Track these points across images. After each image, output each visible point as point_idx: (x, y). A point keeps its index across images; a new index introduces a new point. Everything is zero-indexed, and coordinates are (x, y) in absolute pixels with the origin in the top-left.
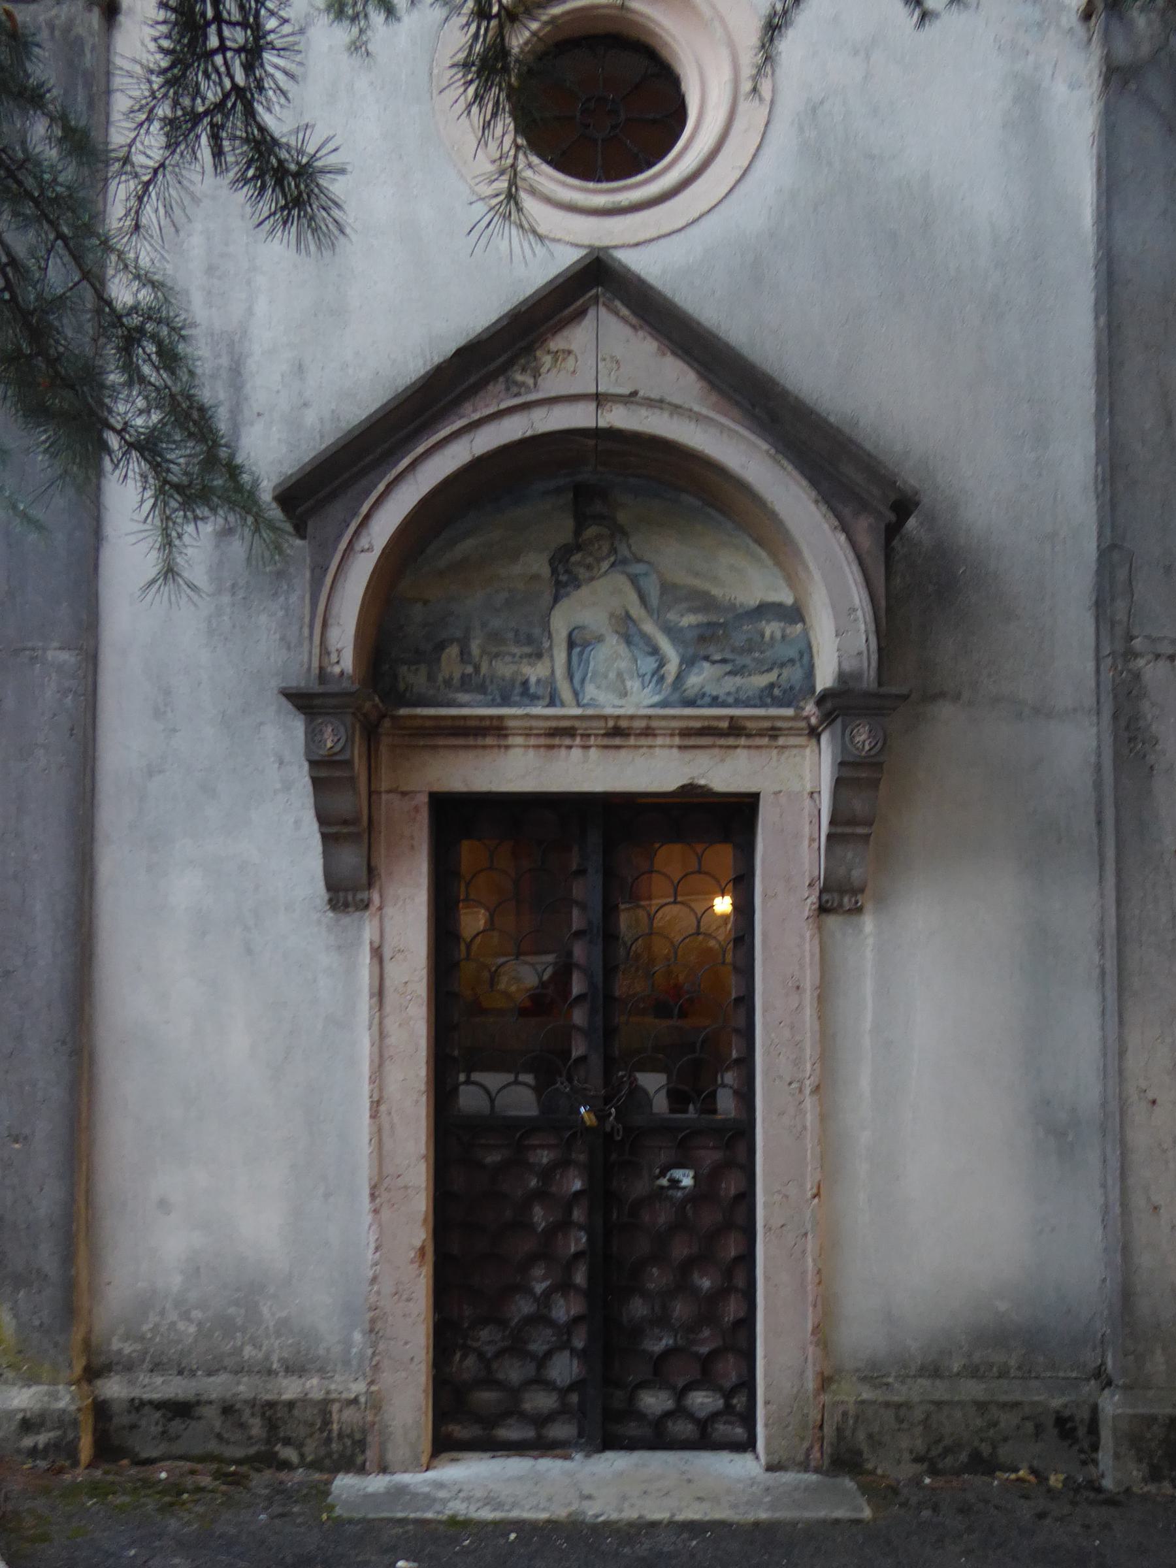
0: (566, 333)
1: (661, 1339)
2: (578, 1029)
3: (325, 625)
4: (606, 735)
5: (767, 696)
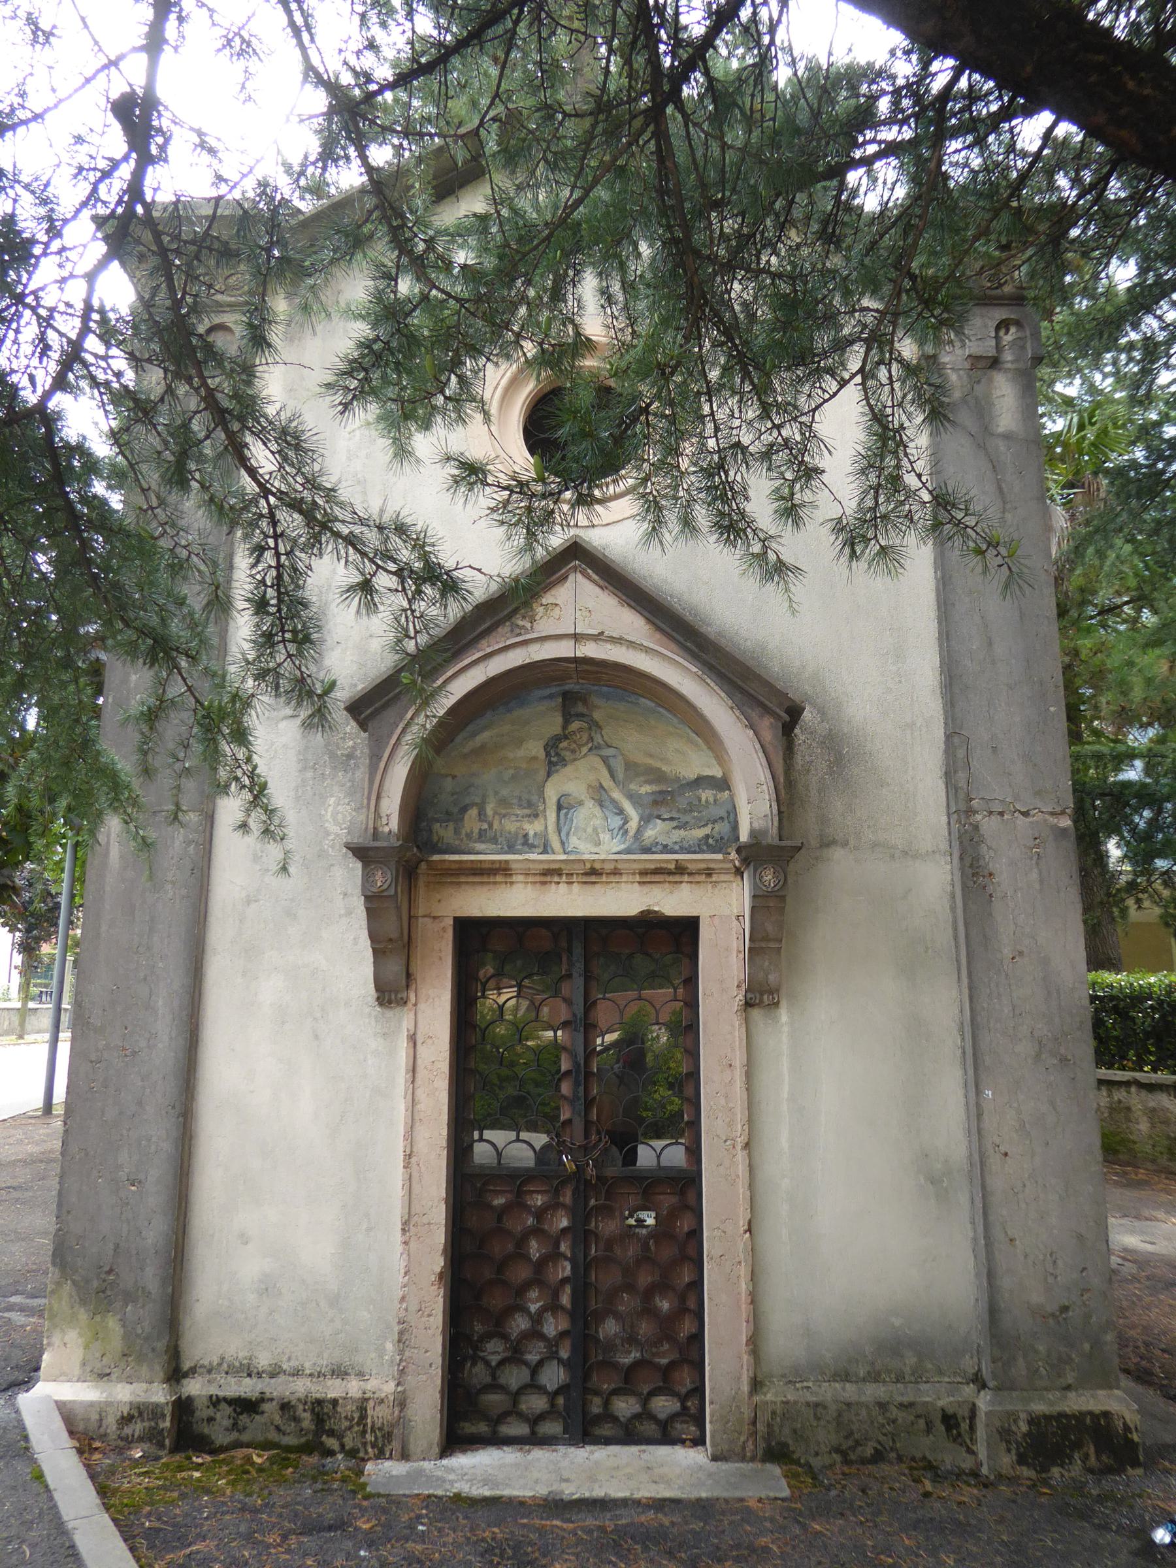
0: (553, 592)
1: (630, 1352)
2: (565, 1098)
3: (378, 797)
4: (586, 874)
5: (704, 845)
